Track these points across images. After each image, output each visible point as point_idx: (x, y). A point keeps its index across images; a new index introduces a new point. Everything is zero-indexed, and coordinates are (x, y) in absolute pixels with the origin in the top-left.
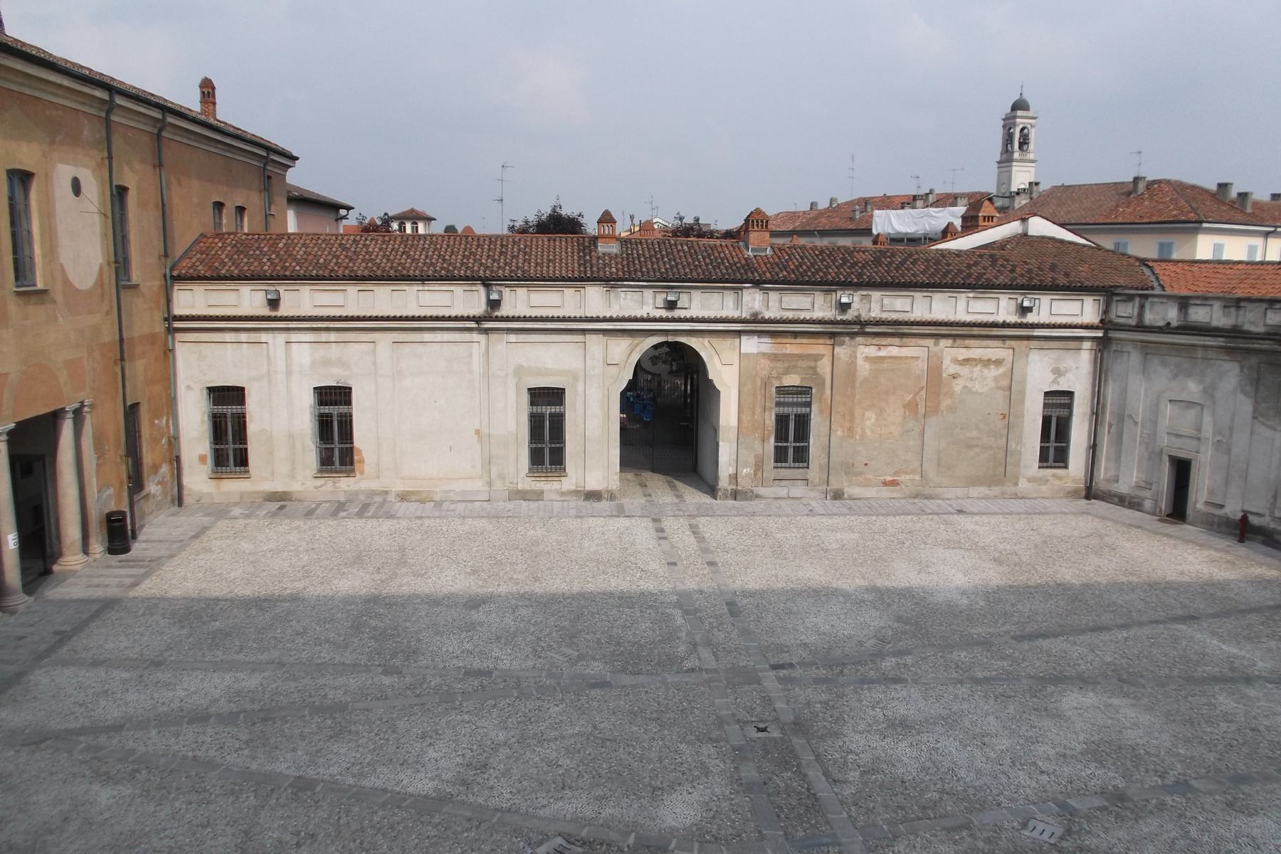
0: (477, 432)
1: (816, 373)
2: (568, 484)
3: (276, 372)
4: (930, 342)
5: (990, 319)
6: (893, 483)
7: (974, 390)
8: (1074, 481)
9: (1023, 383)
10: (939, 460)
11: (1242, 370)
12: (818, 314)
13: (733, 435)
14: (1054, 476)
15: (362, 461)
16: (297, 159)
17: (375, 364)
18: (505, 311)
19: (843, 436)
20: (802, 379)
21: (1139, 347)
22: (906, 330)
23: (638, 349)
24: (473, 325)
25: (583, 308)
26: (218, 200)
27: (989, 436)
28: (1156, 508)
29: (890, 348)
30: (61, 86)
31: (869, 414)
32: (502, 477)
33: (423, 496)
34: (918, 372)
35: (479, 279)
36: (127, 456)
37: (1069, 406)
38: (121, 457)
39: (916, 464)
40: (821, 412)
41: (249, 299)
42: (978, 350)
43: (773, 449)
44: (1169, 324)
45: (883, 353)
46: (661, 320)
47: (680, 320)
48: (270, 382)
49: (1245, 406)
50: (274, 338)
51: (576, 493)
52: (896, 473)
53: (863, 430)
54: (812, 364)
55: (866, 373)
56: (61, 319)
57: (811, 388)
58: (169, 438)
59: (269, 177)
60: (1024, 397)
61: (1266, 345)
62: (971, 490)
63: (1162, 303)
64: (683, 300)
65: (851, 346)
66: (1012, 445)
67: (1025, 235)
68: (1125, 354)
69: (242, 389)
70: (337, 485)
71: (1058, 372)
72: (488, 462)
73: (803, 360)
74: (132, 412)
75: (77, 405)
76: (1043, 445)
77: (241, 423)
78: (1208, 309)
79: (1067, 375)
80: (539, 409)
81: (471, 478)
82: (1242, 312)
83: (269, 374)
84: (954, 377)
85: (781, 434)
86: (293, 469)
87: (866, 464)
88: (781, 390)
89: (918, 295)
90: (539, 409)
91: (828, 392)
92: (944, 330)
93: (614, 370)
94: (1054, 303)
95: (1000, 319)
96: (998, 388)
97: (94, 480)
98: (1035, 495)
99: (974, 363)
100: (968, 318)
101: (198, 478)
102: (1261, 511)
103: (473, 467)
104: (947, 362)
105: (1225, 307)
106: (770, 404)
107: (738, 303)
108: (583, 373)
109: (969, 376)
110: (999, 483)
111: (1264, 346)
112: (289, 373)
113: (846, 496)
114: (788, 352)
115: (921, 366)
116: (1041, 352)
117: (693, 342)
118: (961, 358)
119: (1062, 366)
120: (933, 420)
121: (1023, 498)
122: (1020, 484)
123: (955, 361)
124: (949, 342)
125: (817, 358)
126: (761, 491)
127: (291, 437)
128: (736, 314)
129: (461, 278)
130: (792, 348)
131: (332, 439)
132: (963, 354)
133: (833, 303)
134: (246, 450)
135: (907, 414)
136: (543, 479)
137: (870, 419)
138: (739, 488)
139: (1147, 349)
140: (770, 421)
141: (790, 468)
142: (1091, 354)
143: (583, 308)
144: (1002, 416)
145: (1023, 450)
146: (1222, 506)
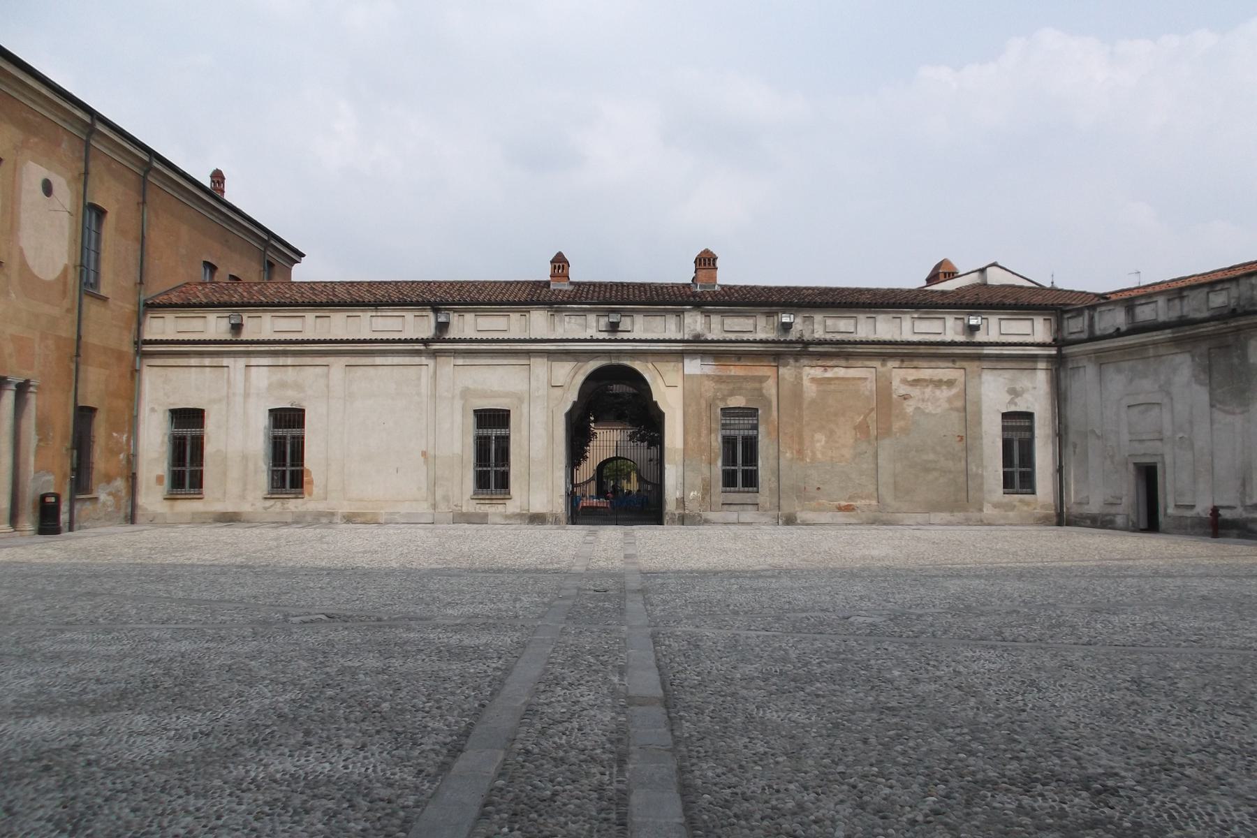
0: (424, 454)
1: (762, 395)
2: (512, 507)
3: (234, 394)
4: (877, 364)
5: (938, 338)
6: (848, 509)
7: (927, 411)
8: (1043, 507)
9: (978, 403)
10: (895, 483)
11: (1193, 360)
12: (761, 335)
13: (679, 458)
14: (1021, 501)
15: (311, 482)
16: (303, 255)
17: (328, 386)
18: (453, 333)
19: (792, 459)
20: (748, 401)
21: (1093, 359)
22: (850, 349)
23: (582, 371)
24: (421, 347)
25: (528, 332)
26: (209, 261)
27: (947, 459)
28: (1128, 522)
29: (836, 369)
30: (39, 94)
31: (818, 436)
32: (446, 498)
33: (369, 517)
34: (867, 393)
35: (428, 303)
36: (73, 448)
37: (1031, 429)
38: (67, 450)
39: (872, 488)
40: (769, 434)
41: (214, 325)
42: (927, 372)
43: (720, 473)
44: (1118, 329)
45: (830, 374)
46: (604, 340)
47: (622, 341)
48: (228, 404)
49: (1201, 395)
50: (235, 361)
51: (520, 516)
52: (850, 498)
53: (814, 453)
54: (757, 385)
55: (814, 395)
56: (13, 295)
57: (757, 410)
58: (128, 456)
59: (271, 265)
60: (981, 418)
61: (1209, 328)
62: (932, 515)
63: (1110, 310)
64: (625, 323)
65: (795, 367)
66: (973, 468)
67: (985, 284)
68: (1082, 370)
69: (202, 411)
70: (286, 506)
71: (1014, 393)
72: (434, 483)
73: (748, 382)
74: (84, 415)
75: (21, 380)
76: (1006, 470)
77: (198, 444)
78: (1152, 306)
79: (1025, 396)
80: (485, 432)
81: (416, 500)
82: (1185, 302)
83: (228, 397)
84: (905, 397)
85: (729, 458)
86: (245, 490)
87: (819, 488)
88: (727, 412)
89: (862, 317)
90: (485, 432)
91: (775, 414)
92: (889, 349)
93: (558, 392)
94: (1003, 322)
95: (948, 338)
96: (952, 409)
97: (32, 459)
98: (1002, 522)
99: (925, 384)
100: (916, 338)
101: (152, 497)
102: (1232, 504)
103: (419, 489)
104: (896, 383)
105: (1169, 300)
106: (716, 425)
107: (680, 327)
108: (528, 396)
109: (921, 397)
110: (964, 509)
111: (1210, 329)
112: (247, 395)
113: (799, 521)
114: (732, 373)
115: (870, 386)
116: (995, 372)
117: (637, 365)
118: (910, 378)
119: (1018, 387)
120: (886, 443)
121: (989, 524)
122: (985, 510)
123: (904, 381)
124: (897, 363)
125: (762, 379)
126: (711, 515)
127: (245, 458)
128: (679, 337)
129: (411, 304)
130: (735, 370)
131: (284, 460)
132: (912, 374)
133: (776, 325)
134: (201, 472)
135: (858, 436)
136: (487, 502)
137: (818, 441)
138: (687, 512)
139: (1101, 359)
140: (717, 442)
141: (739, 492)
142: (1047, 374)
143: (528, 332)
144: (959, 439)
145: (985, 473)
146: (1193, 507)
